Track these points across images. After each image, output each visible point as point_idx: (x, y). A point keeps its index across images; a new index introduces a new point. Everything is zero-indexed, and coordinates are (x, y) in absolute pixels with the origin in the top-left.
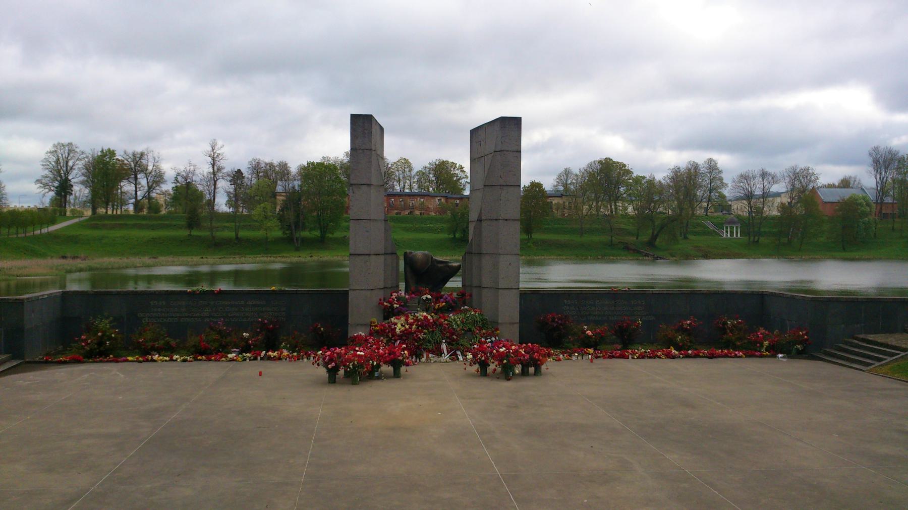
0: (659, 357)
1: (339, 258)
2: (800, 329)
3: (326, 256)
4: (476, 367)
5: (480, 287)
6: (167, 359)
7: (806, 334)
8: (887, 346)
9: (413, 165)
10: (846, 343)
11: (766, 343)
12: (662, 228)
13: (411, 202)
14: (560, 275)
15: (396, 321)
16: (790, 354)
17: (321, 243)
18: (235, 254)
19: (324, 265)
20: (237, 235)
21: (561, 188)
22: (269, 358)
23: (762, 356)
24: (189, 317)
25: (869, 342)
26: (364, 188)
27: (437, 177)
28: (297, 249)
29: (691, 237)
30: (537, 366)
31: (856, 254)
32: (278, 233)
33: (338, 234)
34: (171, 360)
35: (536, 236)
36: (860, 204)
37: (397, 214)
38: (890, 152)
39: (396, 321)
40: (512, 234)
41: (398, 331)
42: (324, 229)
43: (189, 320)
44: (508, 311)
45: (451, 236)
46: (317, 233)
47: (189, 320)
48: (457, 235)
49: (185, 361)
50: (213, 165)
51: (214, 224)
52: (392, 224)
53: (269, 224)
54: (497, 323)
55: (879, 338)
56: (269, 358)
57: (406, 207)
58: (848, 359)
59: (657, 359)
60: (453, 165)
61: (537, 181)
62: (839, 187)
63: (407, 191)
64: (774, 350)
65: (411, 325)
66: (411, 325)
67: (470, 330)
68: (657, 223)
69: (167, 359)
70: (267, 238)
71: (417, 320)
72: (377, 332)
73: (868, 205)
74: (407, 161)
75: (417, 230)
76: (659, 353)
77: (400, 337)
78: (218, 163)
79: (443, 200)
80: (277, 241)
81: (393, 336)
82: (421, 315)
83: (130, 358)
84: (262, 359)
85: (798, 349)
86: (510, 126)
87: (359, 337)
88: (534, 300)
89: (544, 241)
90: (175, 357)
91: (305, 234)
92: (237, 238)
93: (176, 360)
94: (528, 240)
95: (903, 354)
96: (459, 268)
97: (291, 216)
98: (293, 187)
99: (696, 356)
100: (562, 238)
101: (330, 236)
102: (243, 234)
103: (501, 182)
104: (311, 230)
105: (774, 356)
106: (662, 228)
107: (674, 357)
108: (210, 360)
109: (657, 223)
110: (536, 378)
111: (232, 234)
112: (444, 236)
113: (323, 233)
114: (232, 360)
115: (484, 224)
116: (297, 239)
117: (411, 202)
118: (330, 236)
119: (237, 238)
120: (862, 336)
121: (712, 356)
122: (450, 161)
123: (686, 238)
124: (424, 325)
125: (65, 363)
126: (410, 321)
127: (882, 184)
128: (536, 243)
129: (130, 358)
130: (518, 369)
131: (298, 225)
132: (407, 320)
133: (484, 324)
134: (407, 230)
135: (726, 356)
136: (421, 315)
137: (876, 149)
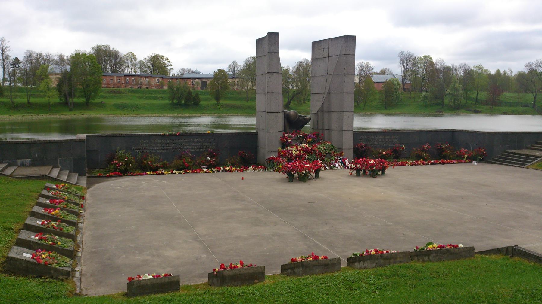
0: (420, 165)
1: (102, 116)
2: (480, 148)
3: (91, 114)
4: (355, 172)
5: (330, 130)
6: (170, 172)
7: (484, 151)
8: (527, 155)
9: (137, 57)
10: (503, 155)
11: (466, 156)
12: (293, 97)
13: (141, 80)
14: (379, 123)
15: (291, 149)
16: (481, 161)
17: (86, 106)
18: (31, 113)
19: (88, 120)
20: (28, 101)
21: (231, 73)
22: (226, 171)
23: (465, 162)
24: (161, 149)
25: (515, 153)
26: (275, 74)
27: (153, 65)
28: (71, 110)
29: (306, 102)
30: (383, 169)
31: (393, 111)
32: (57, 100)
33: (97, 100)
34: (172, 173)
35: (222, 102)
36: (395, 84)
37: (131, 87)
38: (409, 55)
39: (291, 149)
40: (349, 101)
41: (294, 154)
42: (88, 99)
43: (162, 151)
44: (348, 143)
45: (171, 102)
46: (82, 100)
47: (162, 151)
48: (175, 101)
49: (180, 173)
50: (3, 54)
51: (13, 94)
52: (130, 94)
53: (51, 94)
54: (342, 149)
55: (516, 151)
56: (147, 174)
57: (137, 84)
58: (509, 162)
59: (419, 166)
60: (162, 57)
61: (222, 69)
62: (379, 74)
63: (133, 73)
64: (470, 159)
65: (300, 151)
66: (300, 151)
67: (329, 153)
68: (291, 94)
69: (170, 172)
70: (49, 103)
71: (302, 148)
72: (282, 155)
73: (399, 84)
74: (133, 54)
75: (146, 98)
76: (419, 163)
77: (295, 157)
78: (5, 53)
79: (160, 80)
80: (56, 105)
81: (291, 157)
82: (304, 145)
83: (148, 173)
84: (222, 171)
85: (480, 158)
86: (273, 37)
87: (273, 158)
88: (361, 135)
89: (227, 105)
90: (174, 172)
91: (76, 100)
92: (29, 103)
93: (175, 173)
94: (218, 104)
95: (539, 159)
96: (310, 120)
97: (66, 88)
98: (66, 70)
99: (436, 163)
100: (238, 103)
101: (92, 101)
102: (32, 100)
103: (345, 72)
104: (79, 97)
105: (471, 162)
106: (293, 97)
107: (426, 164)
108: (194, 173)
109: (291, 94)
110: (383, 176)
111: (25, 100)
112: (167, 102)
113: (88, 99)
114: (206, 172)
115: (332, 95)
116: (71, 104)
117: (141, 80)
118: (92, 101)
119: (29, 103)
120: (510, 151)
121: (443, 163)
122: (161, 55)
123: (304, 103)
124: (306, 151)
125: (111, 177)
126: (299, 149)
127: (405, 72)
128: (222, 106)
129: (148, 173)
130: (380, 173)
131: (71, 94)
132: (297, 149)
133: (334, 149)
134: (140, 98)
135: (449, 163)
136: (304, 145)
137: (402, 53)
